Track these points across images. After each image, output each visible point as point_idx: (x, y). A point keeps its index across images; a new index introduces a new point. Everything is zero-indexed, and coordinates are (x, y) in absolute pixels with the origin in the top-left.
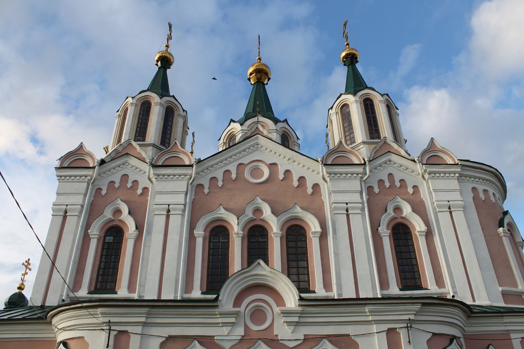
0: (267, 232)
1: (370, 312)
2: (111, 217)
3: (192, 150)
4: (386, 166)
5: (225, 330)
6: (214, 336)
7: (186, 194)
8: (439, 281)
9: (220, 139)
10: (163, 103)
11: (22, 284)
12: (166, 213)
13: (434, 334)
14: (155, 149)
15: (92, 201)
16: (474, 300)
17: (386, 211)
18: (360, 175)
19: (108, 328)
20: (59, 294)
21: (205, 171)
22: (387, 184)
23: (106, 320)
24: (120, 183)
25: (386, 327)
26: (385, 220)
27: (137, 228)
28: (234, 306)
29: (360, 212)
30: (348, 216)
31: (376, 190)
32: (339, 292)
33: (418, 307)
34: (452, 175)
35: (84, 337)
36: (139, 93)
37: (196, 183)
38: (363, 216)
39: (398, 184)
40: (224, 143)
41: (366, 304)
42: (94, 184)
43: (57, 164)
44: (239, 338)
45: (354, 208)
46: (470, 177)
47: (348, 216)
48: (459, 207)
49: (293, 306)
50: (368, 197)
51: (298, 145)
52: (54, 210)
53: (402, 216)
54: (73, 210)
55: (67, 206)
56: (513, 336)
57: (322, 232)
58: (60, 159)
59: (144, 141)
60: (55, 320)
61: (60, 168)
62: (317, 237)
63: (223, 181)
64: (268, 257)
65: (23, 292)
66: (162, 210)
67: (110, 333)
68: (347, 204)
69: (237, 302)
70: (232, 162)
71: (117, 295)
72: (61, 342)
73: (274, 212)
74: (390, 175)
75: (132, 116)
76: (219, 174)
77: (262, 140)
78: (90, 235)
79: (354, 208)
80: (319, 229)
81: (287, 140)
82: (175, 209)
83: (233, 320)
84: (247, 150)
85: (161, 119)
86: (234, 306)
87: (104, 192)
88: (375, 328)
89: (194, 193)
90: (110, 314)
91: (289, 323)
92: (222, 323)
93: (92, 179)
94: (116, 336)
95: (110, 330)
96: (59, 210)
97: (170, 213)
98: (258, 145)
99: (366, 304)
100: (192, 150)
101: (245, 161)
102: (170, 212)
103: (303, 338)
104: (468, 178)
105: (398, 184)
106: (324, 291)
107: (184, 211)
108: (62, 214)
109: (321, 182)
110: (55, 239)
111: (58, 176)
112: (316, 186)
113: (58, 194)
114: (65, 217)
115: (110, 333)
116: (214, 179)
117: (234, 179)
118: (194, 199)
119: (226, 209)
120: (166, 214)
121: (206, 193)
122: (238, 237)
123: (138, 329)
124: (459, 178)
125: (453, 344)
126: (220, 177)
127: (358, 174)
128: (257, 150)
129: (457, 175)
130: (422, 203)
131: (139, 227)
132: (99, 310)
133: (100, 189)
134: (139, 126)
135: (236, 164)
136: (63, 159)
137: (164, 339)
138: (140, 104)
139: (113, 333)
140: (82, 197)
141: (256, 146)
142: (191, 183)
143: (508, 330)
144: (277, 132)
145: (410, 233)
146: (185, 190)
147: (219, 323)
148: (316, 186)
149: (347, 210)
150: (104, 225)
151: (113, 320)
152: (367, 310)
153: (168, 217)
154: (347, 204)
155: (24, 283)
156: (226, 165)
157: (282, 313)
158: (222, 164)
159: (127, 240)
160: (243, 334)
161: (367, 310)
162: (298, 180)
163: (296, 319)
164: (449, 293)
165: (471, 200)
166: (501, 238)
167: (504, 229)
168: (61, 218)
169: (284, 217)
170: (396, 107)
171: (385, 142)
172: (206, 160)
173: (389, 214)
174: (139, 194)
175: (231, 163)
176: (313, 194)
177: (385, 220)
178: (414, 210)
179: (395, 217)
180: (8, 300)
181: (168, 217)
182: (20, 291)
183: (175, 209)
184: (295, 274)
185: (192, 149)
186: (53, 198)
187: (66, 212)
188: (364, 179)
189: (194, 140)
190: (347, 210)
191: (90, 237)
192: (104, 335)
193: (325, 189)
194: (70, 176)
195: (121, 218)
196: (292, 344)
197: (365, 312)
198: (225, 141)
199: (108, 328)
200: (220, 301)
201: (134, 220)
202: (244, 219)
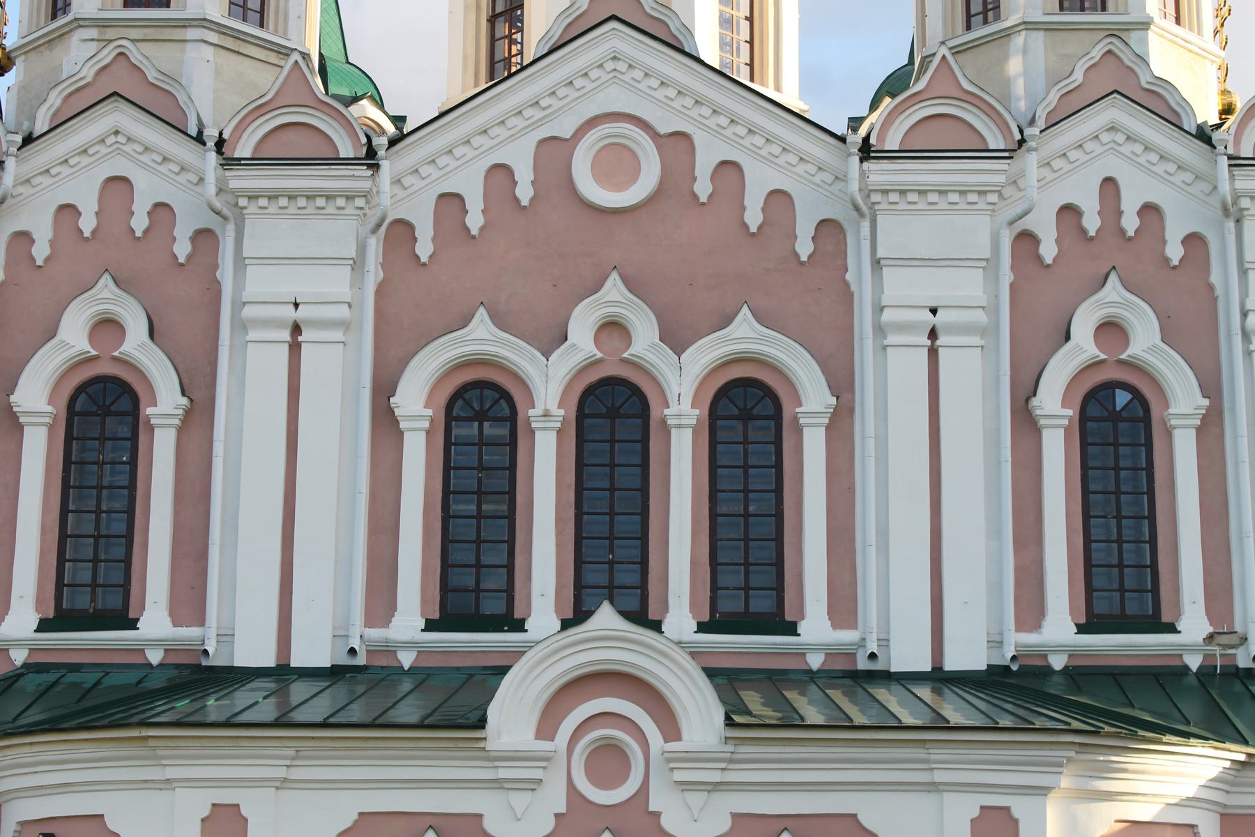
2: (86, 350)
12: (288, 338)
24: (763, 210)
30: (933, 352)
32: (883, 636)
35: (103, 815)
39: (1130, 223)
53: (1121, 357)
57: (836, 406)
62: (559, 421)
68: (934, 311)
71: (136, 631)
74: (1109, 185)
78: (1042, 422)
97: (300, 339)
102: (301, 335)
105: (1130, 223)
112: (1194, 241)
120: (288, 342)
149: (933, 334)
150: (63, 373)
162: (1140, 213)
173: (1079, 349)
175: (771, 160)
179: (594, 358)
184: (457, 545)
190: (933, 334)
191: (533, 426)
195: (120, 353)
201: (1058, 350)
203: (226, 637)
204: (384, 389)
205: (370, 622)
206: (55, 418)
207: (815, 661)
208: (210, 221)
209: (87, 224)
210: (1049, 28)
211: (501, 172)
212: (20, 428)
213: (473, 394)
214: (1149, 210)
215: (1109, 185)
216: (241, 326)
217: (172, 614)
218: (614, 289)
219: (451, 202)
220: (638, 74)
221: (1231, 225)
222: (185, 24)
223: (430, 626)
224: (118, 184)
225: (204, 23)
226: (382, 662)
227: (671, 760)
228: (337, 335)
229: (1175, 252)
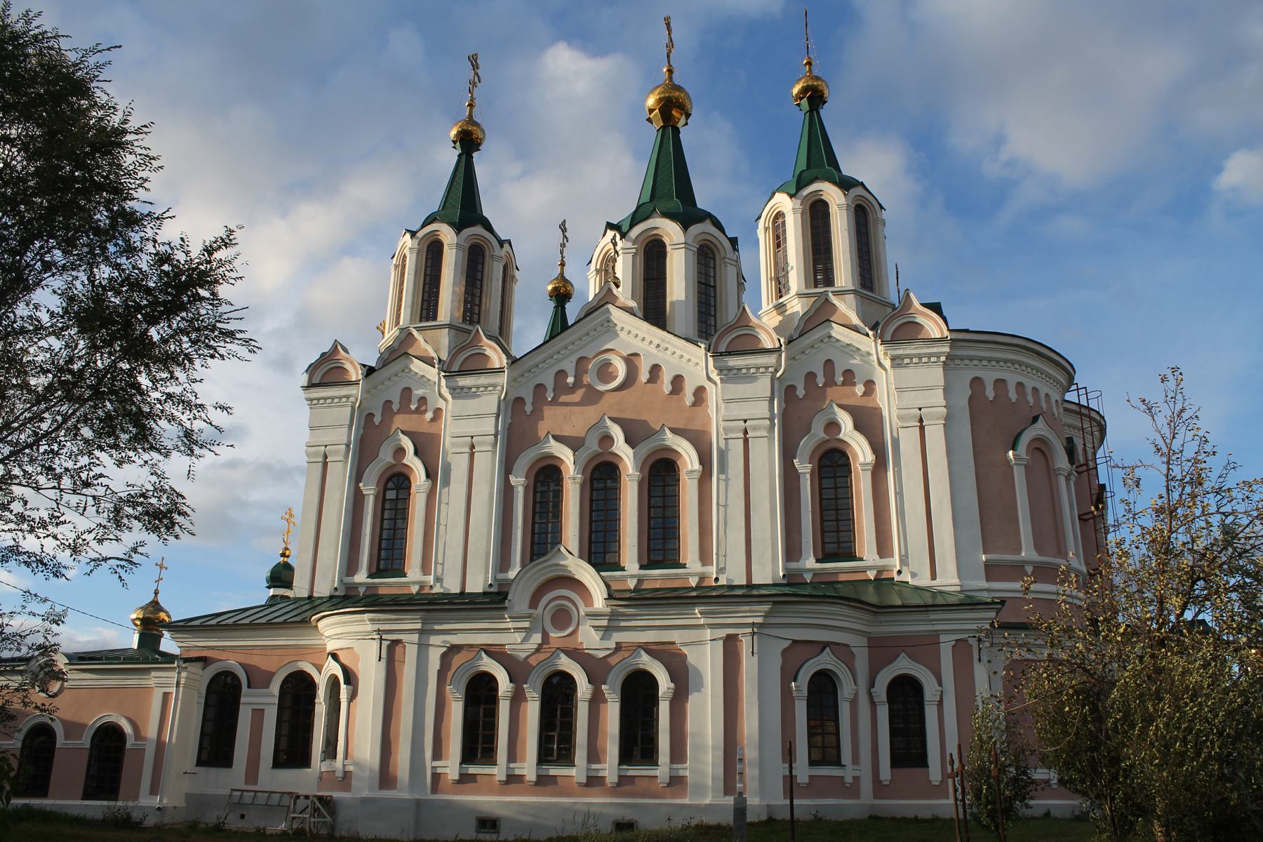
0: (620, 473)
1: (700, 613)
4: (823, 345)
5: (518, 637)
6: (504, 645)
7: (497, 418)
8: (883, 547)
9: (590, 262)
10: (462, 244)
11: (286, 549)
12: (468, 451)
13: (795, 642)
14: (453, 332)
15: (362, 436)
16: (934, 577)
18: (770, 370)
19: (378, 637)
20: (330, 579)
21: (526, 375)
23: (376, 627)
25: (723, 633)
26: (806, 445)
27: (428, 476)
28: (530, 607)
29: (765, 434)
31: (801, 392)
33: (766, 607)
34: (933, 359)
36: (423, 226)
37: (512, 397)
38: (771, 439)
40: (596, 269)
41: (695, 603)
42: (362, 407)
44: (535, 647)
45: (755, 428)
46: (971, 359)
47: (746, 441)
48: (938, 419)
49: (601, 606)
50: (784, 405)
51: (735, 263)
52: (308, 455)
54: (336, 453)
55: (326, 446)
58: (307, 371)
59: (435, 318)
60: (321, 624)
61: (311, 385)
63: (554, 390)
64: (620, 514)
65: (289, 560)
66: (463, 445)
67: (381, 644)
69: (534, 603)
70: (568, 356)
72: (329, 654)
73: (629, 441)
75: (413, 273)
76: (548, 380)
77: (616, 315)
79: (755, 428)
80: (697, 466)
81: (711, 256)
82: (481, 444)
83: (526, 624)
84: (592, 334)
85: (462, 272)
86: (530, 607)
87: (377, 420)
88: (708, 634)
90: (379, 620)
91: (596, 628)
92: (514, 629)
93: (357, 400)
94: (389, 647)
95: (381, 639)
96: (316, 454)
98: (608, 321)
99: (695, 603)
103: (614, 646)
104: (967, 362)
106: (699, 564)
108: (321, 459)
109: (708, 385)
110: (316, 500)
113: (312, 428)
115: (381, 644)
116: (540, 388)
117: (571, 386)
118: (511, 423)
119: (556, 438)
121: (528, 413)
122: (575, 483)
123: (415, 637)
124: (949, 362)
125: (824, 653)
126: (550, 385)
127: (767, 368)
128: (608, 331)
129: (943, 359)
130: (876, 413)
131: (431, 474)
132: (366, 616)
134: (426, 290)
135: (574, 358)
136: (312, 369)
137: (445, 649)
139: (385, 644)
140: (345, 430)
141: (606, 325)
142: (504, 399)
143: (936, 631)
144: (687, 246)
145: (848, 465)
146: (495, 411)
147: (510, 629)
148: (700, 392)
149: (746, 432)
151: (382, 627)
152: (697, 611)
153: (472, 455)
154: (920, 409)
155: (289, 547)
156: (559, 361)
157: (587, 615)
158: (552, 361)
159: (415, 496)
160: (540, 642)
161: (697, 611)
163: (605, 623)
164: (895, 566)
165: (964, 403)
166: (1011, 468)
167: (1016, 453)
169: (646, 447)
170: (880, 205)
171: (827, 299)
172: (527, 357)
174: (428, 420)
176: (694, 404)
177: (806, 445)
178: (857, 427)
180: (269, 574)
181: (472, 455)
182: (286, 559)
183: (481, 444)
186: (305, 435)
187: (326, 457)
188: (778, 375)
189: (565, 237)
190: (746, 432)
192: (376, 644)
193: (714, 394)
194: (325, 399)
196: (601, 654)
197: (695, 614)
198: (598, 267)
199: (378, 637)
200: (509, 601)
202: (585, 454)
203: (438, 579)
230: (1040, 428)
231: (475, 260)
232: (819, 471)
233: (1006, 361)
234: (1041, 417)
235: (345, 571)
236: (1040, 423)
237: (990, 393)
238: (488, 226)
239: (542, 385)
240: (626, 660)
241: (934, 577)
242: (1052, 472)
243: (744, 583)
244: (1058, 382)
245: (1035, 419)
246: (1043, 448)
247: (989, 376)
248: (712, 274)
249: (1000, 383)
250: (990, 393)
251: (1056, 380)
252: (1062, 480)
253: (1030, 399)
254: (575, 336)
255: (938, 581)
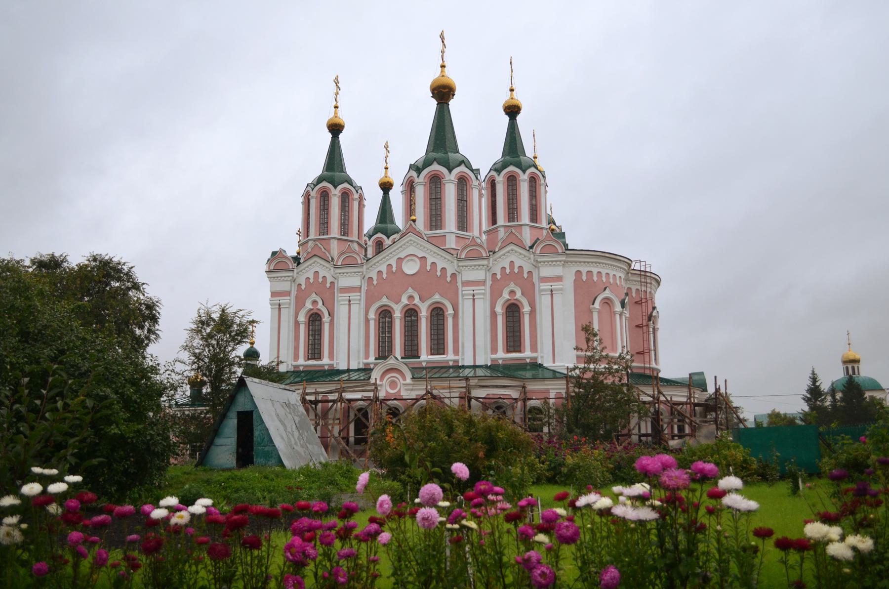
3: (443, 61)
16: (554, 362)
17: (502, 295)
22: (508, 271)
27: (329, 315)
30: (474, 300)
31: (499, 277)
39: (516, 270)
43: (265, 268)
46: (576, 262)
47: (474, 300)
52: (271, 304)
56: (551, 391)
63: (387, 274)
66: (345, 300)
74: (512, 262)
76: (383, 268)
89: (366, 285)
100: (443, 61)
101: (402, 255)
105: (516, 270)
107: (360, 300)
110: (277, 326)
111: (269, 278)
114: (280, 309)
126: (375, 278)
128: (431, 225)
133: (300, 285)
138: (319, 196)
153: (350, 305)
156: (388, 260)
163: (411, 388)
168: (277, 310)
173: (504, 297)
185: (443, 60)
187: (280, 305)
203: (337, 364)
204: (367, 313)
205: (492, 353)
206: (503, 313)
207: (424, 364)
208: (333, 280)
209: (311, 281)
210: (338, 239)
211: (390, 266)
212: (299, 324)
213: (409, 311)
214: (520, 267)
215: (512, 262)
216: (463, 295)
217: (531, 351)
218: (314, 295)
219: (504, 268)
220: (419, 246)
221: (537, 269)
222: (329, 239)
223: (376, 359)
224: (316, 273)
225: (526, 225)
226: (298, 370)
227: (404, 384)
228: (482, 297)
229: (525, 275)
230: (607, 293)
231: (345, 197)
232: (506, 313)
233: (592, 262)
234: (608, 288)
235: (491, 221)
236: (607, 291)
237: (584, 278)
238: (350, 182)
239: (372, 278)
240: (501, 400)
241: (554, 362)
242: (612, 314)
243: (472, 364)
244: (625, 269)
245: (605, 289)
246: (609, 302)
247: (584, 270)
248: (465, 210)
249: (590, 273)
250: (584, 278)
251: (623, 268)
252: (618, 317)
253: (604, 279)
254: (386, 254)
255: (557, 364)
